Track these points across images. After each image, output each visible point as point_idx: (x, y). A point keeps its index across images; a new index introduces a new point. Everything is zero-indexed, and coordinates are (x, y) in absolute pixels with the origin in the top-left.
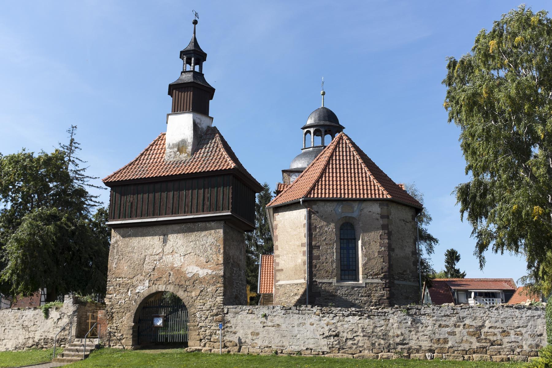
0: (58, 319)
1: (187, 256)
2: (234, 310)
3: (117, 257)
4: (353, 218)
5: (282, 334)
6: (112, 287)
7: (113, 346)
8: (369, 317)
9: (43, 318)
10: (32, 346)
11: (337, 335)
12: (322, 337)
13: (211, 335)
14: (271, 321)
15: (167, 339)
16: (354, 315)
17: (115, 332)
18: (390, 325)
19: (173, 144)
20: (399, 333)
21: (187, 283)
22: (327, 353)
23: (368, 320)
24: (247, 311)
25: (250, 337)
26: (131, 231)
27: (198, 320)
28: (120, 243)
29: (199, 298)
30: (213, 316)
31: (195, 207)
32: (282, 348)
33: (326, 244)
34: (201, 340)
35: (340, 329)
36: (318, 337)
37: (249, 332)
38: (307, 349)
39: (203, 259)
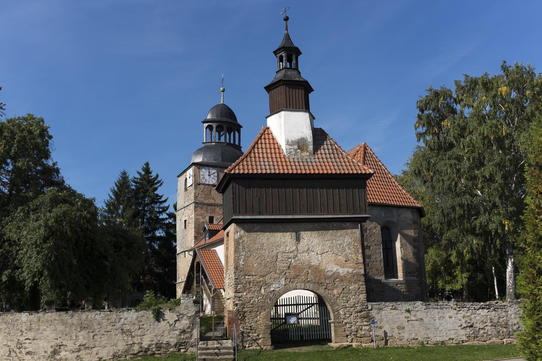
0: (176, 321)
1: (324, 255)
2: (377, 306)
3: (244, 253)
4: (392, 222)
5: (426, 327)
6: (241, 285)
7: (249, 347)
8: (494, 310)
9: (153, 320)
10: (139, 352)
11: (471, 326)
12: (460, 328)
13: (357, 331)
14: (415, 316)
15: (302, 337)
16: (483, 308)
17: (249, 333)
18: (509, 316)
19: (292, 141)
20: (516, 322)
21: (327, 281)
22: (466, 341)
23: (494, 312)
24: (391, 307)
25: (396, 331)
26: (257, 227)
27: (342, 317)
28: (245, 239)
29: (341, 296)
30: (357, 312)
31: (332, 207)
32: (428, 340)
33: (375, 245)
34: (347, 336)
35: (473, 321)
36: (457, 328)
37: (395, 326)
38: (450, 339)
39: (342, 258)
